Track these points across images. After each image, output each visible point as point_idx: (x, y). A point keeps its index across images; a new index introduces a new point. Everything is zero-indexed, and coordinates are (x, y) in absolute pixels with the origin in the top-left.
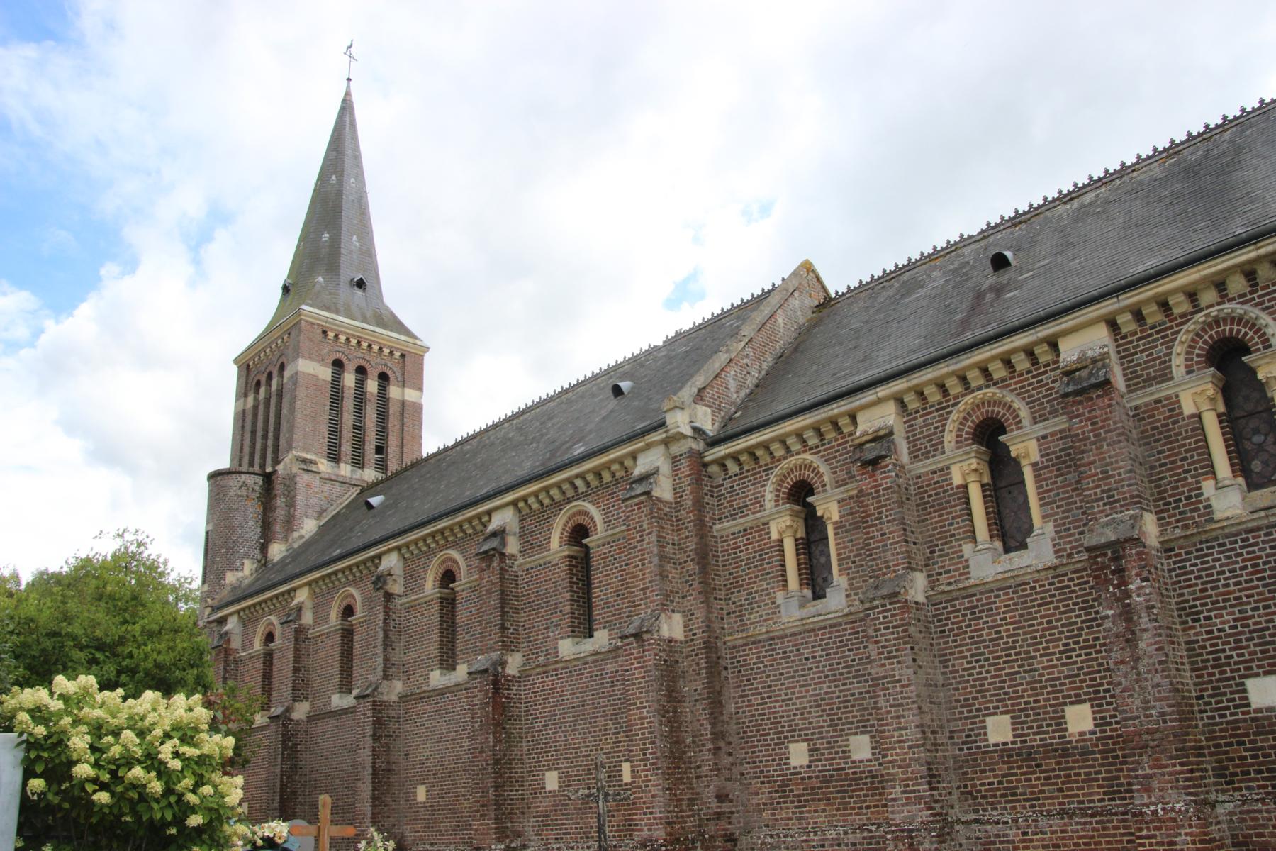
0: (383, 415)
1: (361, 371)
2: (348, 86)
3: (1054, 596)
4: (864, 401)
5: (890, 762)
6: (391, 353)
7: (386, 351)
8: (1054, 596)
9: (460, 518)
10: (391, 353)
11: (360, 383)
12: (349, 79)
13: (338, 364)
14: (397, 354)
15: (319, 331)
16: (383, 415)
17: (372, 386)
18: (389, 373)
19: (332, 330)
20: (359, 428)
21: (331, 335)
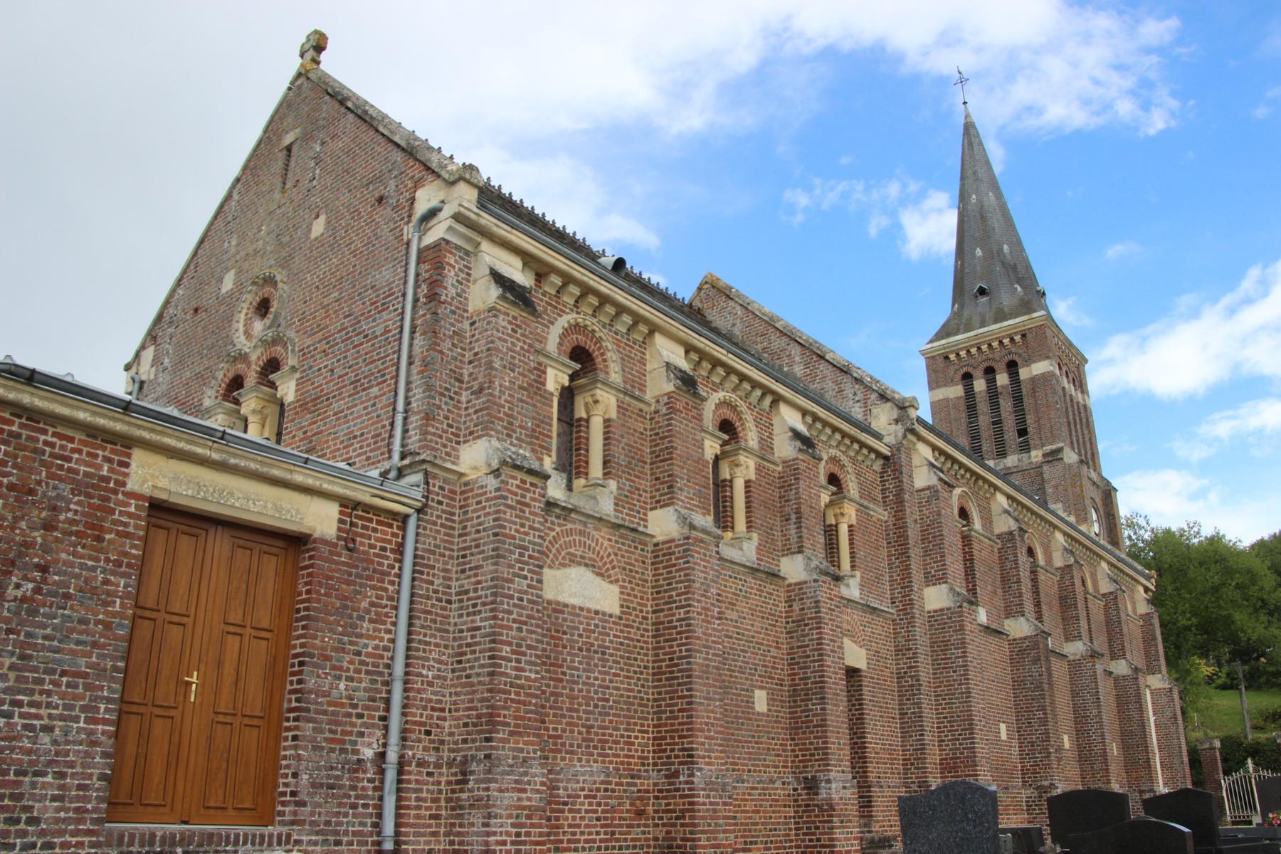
0: (1018, 399)
1: (990, 372)
2: (966, 108)
3: (944, 709)
4: (168, 441)
5: (959, 648)
6: (1012, 340)
7: (1006, 341)
8: (944, 709)
9: (620, 297)
10: (1012, 340)
11: (991, 382)
12: (965, 103)
13: (967, 377)
14: (1017, 338)
15: (941, 360)
16: (1018, 399)
17: (1002, 379)
18: (1016, 358)
19: (952, 352)
20: (997, 423)
21: (952, 357)
